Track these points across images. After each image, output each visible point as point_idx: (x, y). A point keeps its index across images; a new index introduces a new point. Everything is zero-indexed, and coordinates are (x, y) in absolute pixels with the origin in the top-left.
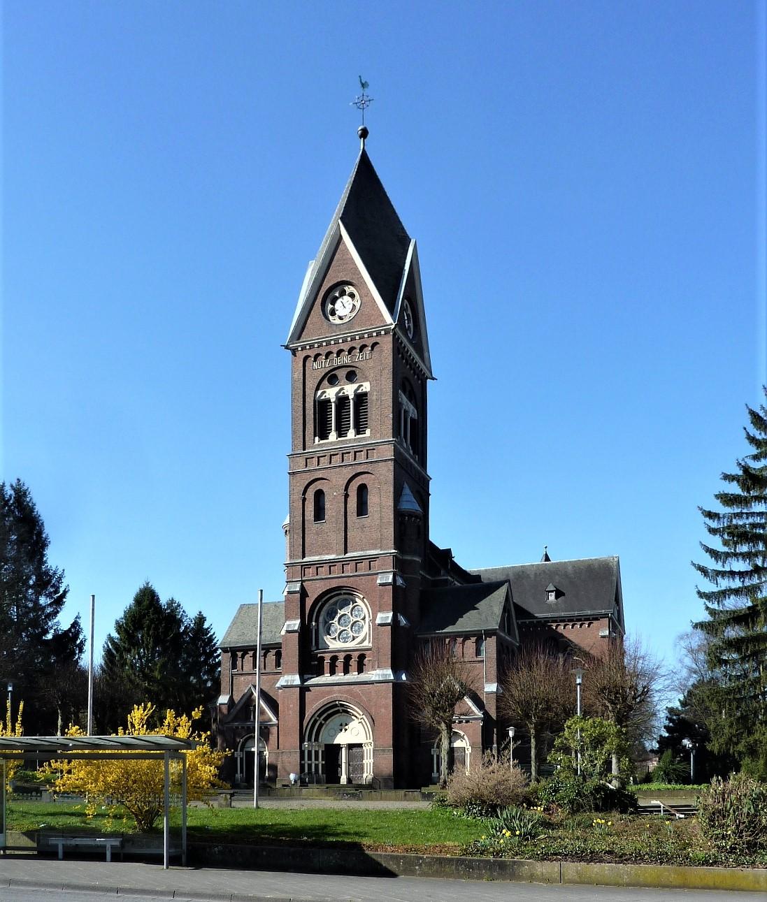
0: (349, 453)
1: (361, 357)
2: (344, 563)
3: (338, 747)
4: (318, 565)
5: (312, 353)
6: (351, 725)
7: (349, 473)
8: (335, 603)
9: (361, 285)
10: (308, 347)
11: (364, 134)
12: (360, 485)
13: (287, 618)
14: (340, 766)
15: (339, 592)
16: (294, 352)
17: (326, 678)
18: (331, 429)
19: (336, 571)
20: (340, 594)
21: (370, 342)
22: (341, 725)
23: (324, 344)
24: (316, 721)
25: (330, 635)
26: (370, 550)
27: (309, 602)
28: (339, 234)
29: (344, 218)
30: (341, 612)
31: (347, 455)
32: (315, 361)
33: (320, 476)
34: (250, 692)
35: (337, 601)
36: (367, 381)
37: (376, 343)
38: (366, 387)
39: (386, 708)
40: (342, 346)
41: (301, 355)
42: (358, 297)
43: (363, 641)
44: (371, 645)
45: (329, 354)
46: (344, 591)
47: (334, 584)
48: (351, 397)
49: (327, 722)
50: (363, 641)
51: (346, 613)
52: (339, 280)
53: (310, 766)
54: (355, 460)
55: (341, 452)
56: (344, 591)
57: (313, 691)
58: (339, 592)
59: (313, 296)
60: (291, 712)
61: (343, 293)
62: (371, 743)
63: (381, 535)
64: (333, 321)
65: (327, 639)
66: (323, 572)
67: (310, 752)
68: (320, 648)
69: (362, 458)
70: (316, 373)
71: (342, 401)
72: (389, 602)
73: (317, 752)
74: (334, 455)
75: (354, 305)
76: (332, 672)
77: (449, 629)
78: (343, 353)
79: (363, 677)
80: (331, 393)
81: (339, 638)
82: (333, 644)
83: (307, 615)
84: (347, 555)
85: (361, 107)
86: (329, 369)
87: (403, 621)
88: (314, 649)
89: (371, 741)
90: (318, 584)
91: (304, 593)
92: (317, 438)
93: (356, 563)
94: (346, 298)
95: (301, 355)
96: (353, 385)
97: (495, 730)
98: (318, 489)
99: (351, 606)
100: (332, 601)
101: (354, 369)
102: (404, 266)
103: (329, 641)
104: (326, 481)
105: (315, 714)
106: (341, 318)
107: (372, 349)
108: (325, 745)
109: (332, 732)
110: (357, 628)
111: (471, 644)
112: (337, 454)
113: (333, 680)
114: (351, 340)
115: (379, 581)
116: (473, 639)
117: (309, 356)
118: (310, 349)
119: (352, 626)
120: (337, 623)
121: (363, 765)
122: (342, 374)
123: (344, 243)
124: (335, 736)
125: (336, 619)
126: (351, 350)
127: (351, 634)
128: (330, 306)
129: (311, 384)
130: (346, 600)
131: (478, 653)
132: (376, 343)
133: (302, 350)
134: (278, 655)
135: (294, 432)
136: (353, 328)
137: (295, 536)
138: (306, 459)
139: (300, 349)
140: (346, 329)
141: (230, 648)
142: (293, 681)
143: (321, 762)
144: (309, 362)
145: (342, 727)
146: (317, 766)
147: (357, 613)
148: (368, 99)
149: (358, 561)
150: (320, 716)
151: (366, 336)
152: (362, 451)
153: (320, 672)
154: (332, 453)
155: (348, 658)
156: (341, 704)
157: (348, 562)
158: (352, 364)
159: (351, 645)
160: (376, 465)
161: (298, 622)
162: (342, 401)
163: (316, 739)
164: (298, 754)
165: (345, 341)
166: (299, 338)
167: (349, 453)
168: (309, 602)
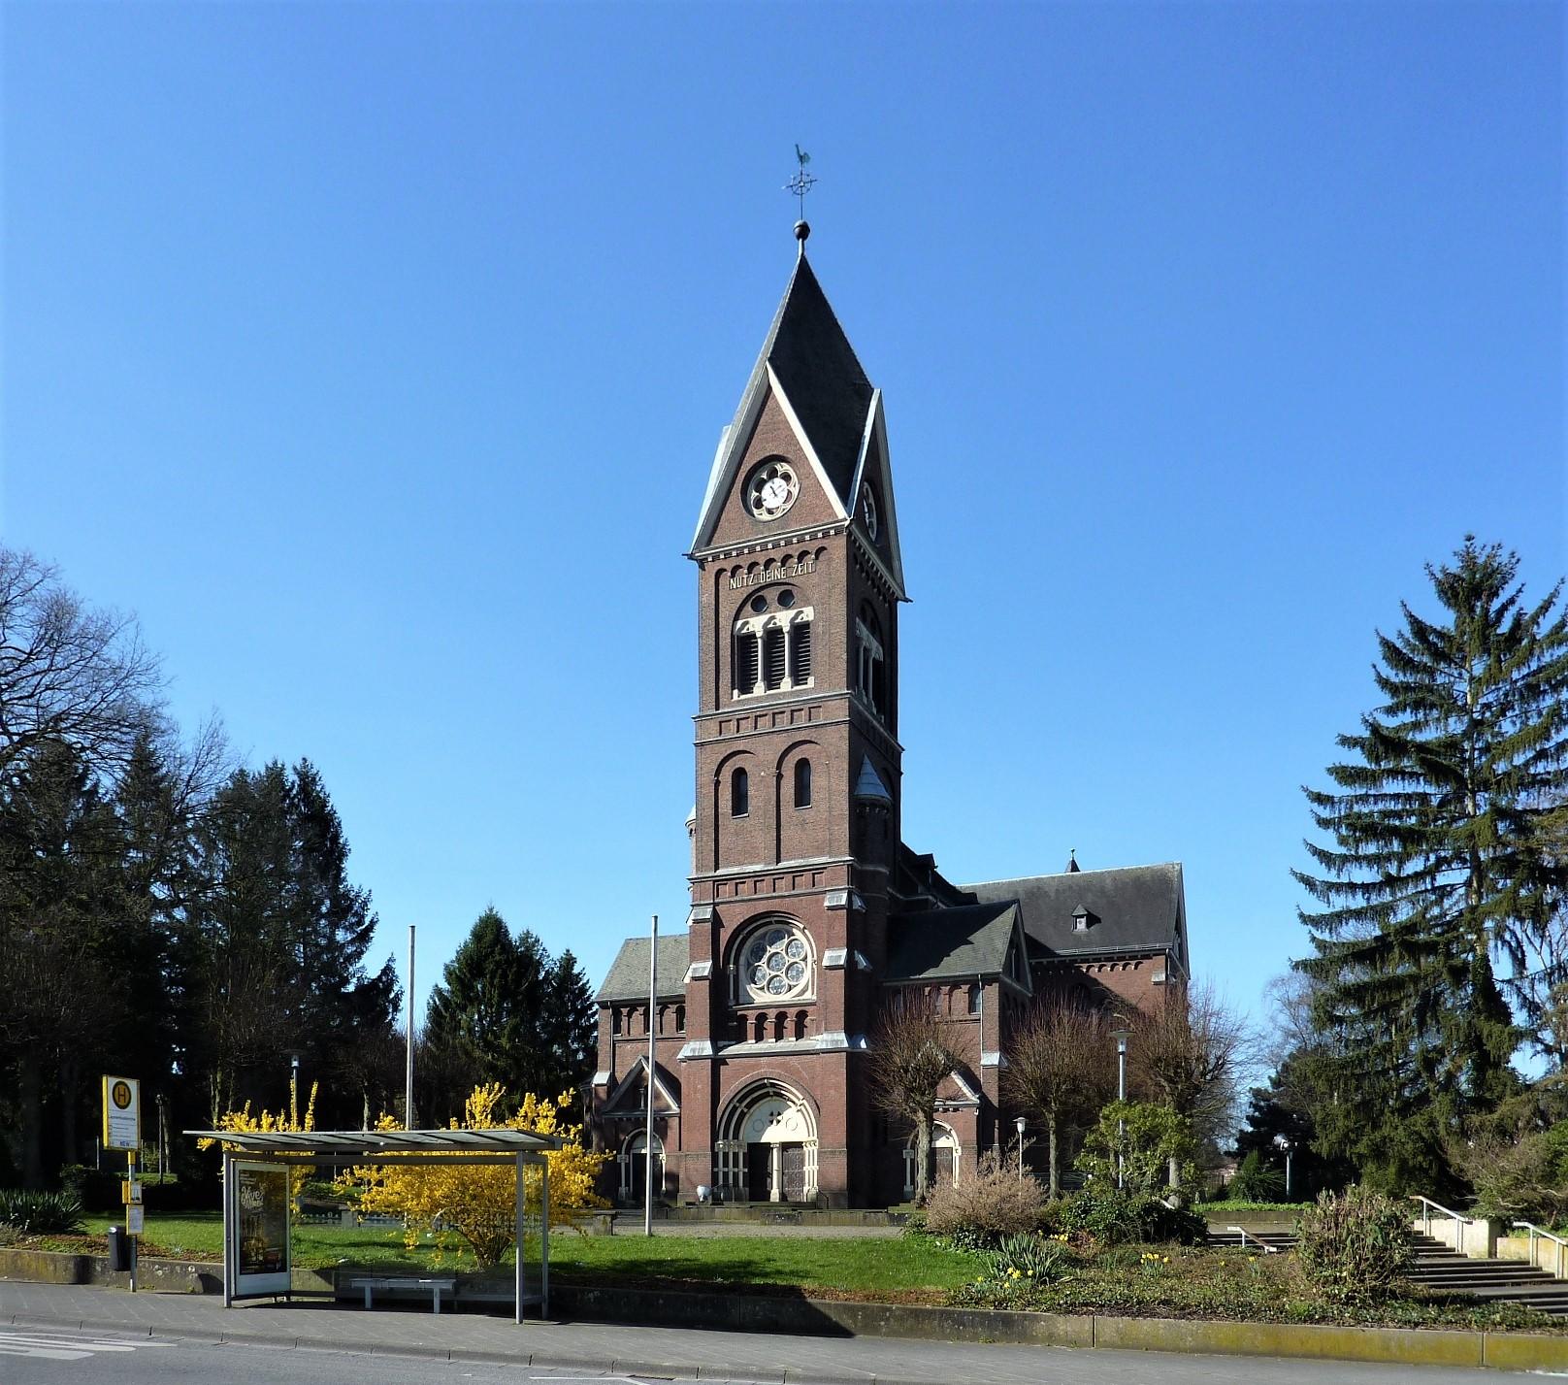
0: (783, 712)
2: (778, 876)
3: (768, 1147)
4: (738, 880)
5: (728, 565)
6: (786, 1115)
7: (783, 742)
10: (722, 557)
11: (804, 232)
13: (693, 959)
14: (770, 1175)
15: (768, 920)
17: (749, 1046)
19: (765, 887)
20: (770, 923)
21: (813, 547)
22: (772, 1114)
23: (746, 551)
24: (735, 1108)
27: (725, 936)
30: (771, 950)
31: (780, 716)
35: (766, 933)
38: (808, 614)
40: (772, 554)
41: (712, 568)
43: (804, 991)
44: (815, 998)
45: (752, 566)
46: (776, 919)
49: (752, 1111)
50: (804, 991)
51: (778, 951)
53: (726, 1175)
55: (754, 714)
56: (776, 919)
58: (768, 920)
59: (729, 480)
60: (699, 1096)
61: (773, 474)
66: (746, 889)
67: (726, 1155)
68: (741, 1002)
69: (801, 720)
71: (773, 635)
73: (736, 1155)
74: (760, 716)
75: (789, 492)
76: (759, 1038)
77: (930, 973)
78: (774, 563)
79: (804, 1044)
80: (756, 624)
82: (760, 997)
84: (780, 865)
85: (799, 192)
87: (862, 962)
89: (815, 1138)
90: (738, 908)
91: (717, 922)
92: (736, 692)
93: (737, 884)
94: (778, 482)
95: (712, 568)
96: (790, 611)
97: (997, 1121)
99: (786, 941)
100: (757, 934)
101: (789, 587)
102: (864, 430)
103: (755, 993)
105: (734, 1098)
106: (770, 511)
107: (817, 558)
109: (758, 1125)
111: (961, 995)
112: (766, 715)
113: (761, 1049)
115: (826, 904)
116: (965, 988)
119: (788, 969)
120: (765, 966)
121: (803, 1173)
122: (771, 595)
124: (762, 1131)
125: (765, 959)
126: (787, 558)
127: (786, 981)
128: (755, 494)
130: (778, 931)
131: (972, 1007)
132: (823, 549)
135: (702, 683)
136: (788, 525)
138: (721, 722)
139: (710, 559)
140: (778, 528)
141: (611, 1002)
142: (703, 1049)
143: (742, 1170)
145: (773, 1117)
146: (736, 1176)
147: (794, 950)
149: (796, 873)
150: (740, 1101)
152: (802, 710)
153: (741, 1038)
154: (758, 713)
155: (781, 1017)
157: (781, 876)
158: (787, 581)
159: (785, 998)
160: (822, 730)
162: (773, 635)
163: (736, 1136)
166: (709, 543)
167: (783, 712)
168: (725, 936)
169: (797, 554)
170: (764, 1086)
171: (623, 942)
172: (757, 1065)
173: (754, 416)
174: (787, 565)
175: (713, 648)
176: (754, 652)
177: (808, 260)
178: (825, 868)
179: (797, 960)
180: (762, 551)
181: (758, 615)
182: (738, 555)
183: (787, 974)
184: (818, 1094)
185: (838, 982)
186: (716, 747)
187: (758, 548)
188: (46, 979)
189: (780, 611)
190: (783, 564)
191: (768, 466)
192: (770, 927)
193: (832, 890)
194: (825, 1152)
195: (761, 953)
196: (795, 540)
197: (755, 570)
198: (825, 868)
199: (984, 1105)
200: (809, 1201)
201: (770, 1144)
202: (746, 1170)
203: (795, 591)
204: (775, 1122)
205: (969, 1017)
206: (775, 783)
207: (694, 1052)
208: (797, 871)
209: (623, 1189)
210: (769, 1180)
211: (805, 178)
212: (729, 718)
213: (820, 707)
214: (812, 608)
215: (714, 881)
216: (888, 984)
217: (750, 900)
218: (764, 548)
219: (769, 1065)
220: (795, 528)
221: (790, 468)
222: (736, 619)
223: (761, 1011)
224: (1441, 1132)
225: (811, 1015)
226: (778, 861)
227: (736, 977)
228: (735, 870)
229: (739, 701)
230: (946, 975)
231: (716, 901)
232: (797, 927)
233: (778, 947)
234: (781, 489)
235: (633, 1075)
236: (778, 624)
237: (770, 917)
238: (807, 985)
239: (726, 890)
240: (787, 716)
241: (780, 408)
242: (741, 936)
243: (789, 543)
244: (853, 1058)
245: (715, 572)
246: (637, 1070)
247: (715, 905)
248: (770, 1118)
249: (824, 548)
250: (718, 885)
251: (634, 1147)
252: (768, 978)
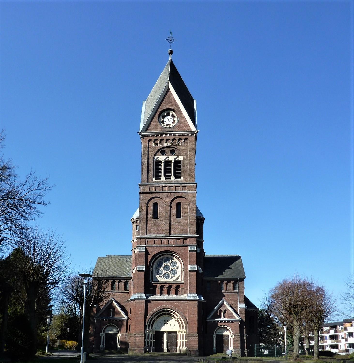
0: (173, 187)
2: (170, 239)
3: (163, 332)
4: (156, 239)
5: (153, 139)
6: (170, 322)
7: (173, 196)
8: (162, 259)
10: (151, 136)
12: (180, 202)
14: (163, 343)
15: (165, 253)
16: (143, 137)
17: (158, 296)
18: (171, 175)
19: (165, 243)
20: (166, 255)
22: (165, 321)
24: (153, 318)
25: (159, 275)
26: (183, 234)
27: (150, 257)
30: (165, 264)
31: (171, 188)
32: (154, 142)
33: (157, 196)
34: (111, 301)
35: (163, 258)
38: (181, 158)
40: (169, 138)
41: (147, 139)
44: (183, 281)
45: (161, 140)
46: (168, 253)
47: (164, 249)
48: (173, 161)
49: (158, 319)
51: (168, 264)
52: (167, 108)
53: (148, 342)
54: (176, 190)
55: (162, 186)
56: (168, 253)
57: (152, 302)
58: (165, 253)
59: (154, 113)
61: (168, 114)
62: (185, 331)
63: (189, 227)
65: (158, 277)
66: (158, 242)
67: (148, 334)
69: (179, 189)
70: (154, 148)
71: (167, 163)
73: (151, 335)
74: (164, 187)
75: (174, 121)
76: (161, 294)
77: (220, 277)
78: (169, 141)
80: (162, 158)
81: (164, 277)
82: (161, 280)
83: (148, 264)
84: (171, 236)
85: (170, 41)
86: (162, 147)
87: (201, 271)
88: (151, 281)
89: (185, 330)
90: (155, 248)
91: (147, 253)
92: (154, 178)
93: (154, 240)
94: (170, 117)
95: (147, 139)
97: (245, 327)
98: (155, 202)
99: (171, 261)
101: (174, 149)
103: (159, 278)
105: (152, 315)
106: (167, 125)
107: (184, 141)
111: (231, 285)
112: (166, 187)
114: (174, 136)
115: (189, 250)
116: (233, 282)
118: (152, 136)
119: (171, 271)
121: (177, 343)
122: (168, 150)
123: (170, 92)
124: (162, 327)
125: (163, 267)
126: (174, 140)
127: (171, 275)
128: (162, 119)
129: (152, 153)
130: (167, 258)
131: (235, 289)
133: (147, 136)
134: (126, 283)
135: (142, 174)
137: (142, 224)
139: (146, 136)
140: (171, 130)
142: (142, 297)
143: (153, 340)
145: (166, 322)
146: (151, 342)
147: (173, 265)
149: (177, 239)
150: (155, 316)
152: (179, 187)
153: (154, 293)
155: (170, 287)
156: (167, 310)
157: (172, 239)
158: (174, 146)
159: (170, 280)
161: (144, 266)
162: (167, 163)
163: (152, 328)
164: (144, 335)
165: (170, 135)
166: (146, 130)
167: (173, 187)
168: (150, 257)
169: (178, 139)
170: (165, 311)
173: (163, 96)
174: (174, 142)
175: (147, 163)
177: (173, 61)
179: (175, 268)
180: (165, 136)
182: (156, 136)
183: (171, 272)
185: (194, 278)
186: (148, 195)
187: (164, 135)
188: (24, 231)
193: (190, 245)
194: (190, 335)
195: (161, 265)
197: (174, 141)
198: (188, 238)
199: (241, 321)
201: (164, 331)
202: (154, 340)
204: (166, 324)
207: (139, 297)
209: (102, 346)
210: (163, 344)
212: (153, 186)
213: (186, 187)
215: (146, 239)
216: (205, 279)
218: (166, 135)
219: (167, 304)
220: (177, 131)
221: (175, 113)
222: (155, 155)
223: (162, 284)
224: (103, 303)
225: (182, 287)
226: (170, 234)
227: (152, 272)
228: (154, 236)
231: (147, 245)
232: (176, 257)
233: (168, 263)
234: (171, 119)
235: (108, 304)
236: (170, 159)
237: (166, 252)
239: (151, 242)
240: (174, 188)
241: (172, 95)
242: (155, 258)
243: (170, 135)
244: (199, 302)
245: (148, 140)
247: (146, 246)
248: (164, 322)
249: (187, 139)
250: (147, 240)
251: (105, 330)
252: (164, 273)
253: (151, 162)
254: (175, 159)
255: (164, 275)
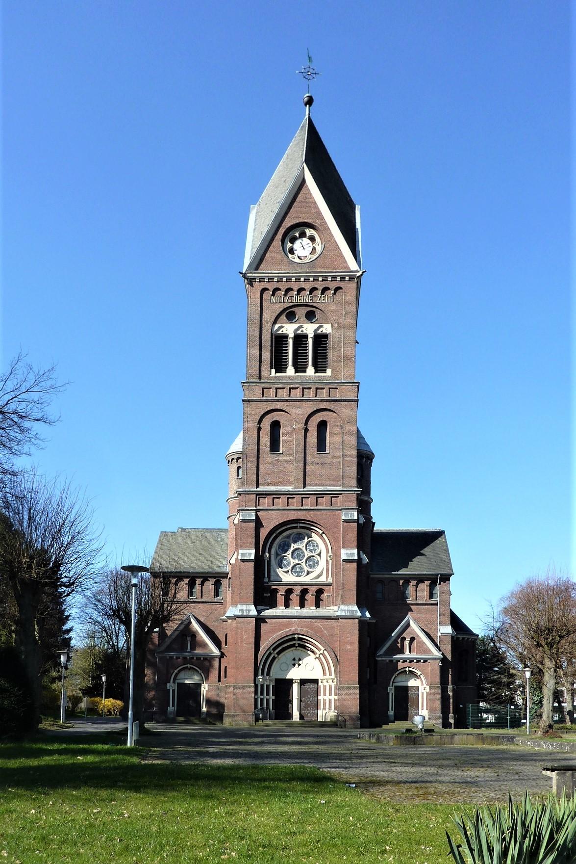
0: (310, 388)
1: (322, 299)
2: (305, 496)
3: (291, 681)
4: (276, 495)
5: (271, 286)
7: (310, 408)
8: (288, 537)
9: (322, 228)
10: (267, 280)
11: (310, 102)
13: (238, 547)
14: (291, 702)
16: (251, 282)
17: (280, 610)
19: (295, 503)
20: (296, 527)
21: (333, 285)
23: (285, 279)
24: (270, 654)
25: (282, 568)
27: (264, 533)
28: (302, 176)
29: (306, 161)
30: (294, 546)
31: (307, 390)
32: (273, 294)
33: (278, 407)
35: (290, 535)
36: (328, 323)
37: (340, 288)
38: (327, 328)
39: (351, 644)
40: (303, 285)
41: (258, 286)
42: (319, 240)
43: (319, 576)
44: (330, 580)
45: (289, 290)
46: (301, 525)
47: (293, 516)
49: (280, 656)
50: (319, 576)
51: (300, 547)
52: (301, 221)
53: (262, 700)
54: (316, 396)
55: (289, 386)
56: (301, 525)
61: (303, 235)
64: (293, 260)
65: (280, 571)
66: (281, 503)
67: (262, 686)
68: (272, 580)
70: (273, 307)
71: (300, 339)
72: (353, 539)
73: (268, 686)
74: (293, 388)
75: (314, 249)
77: (403, 571)
78: (304, 292)
79: (322, 611)
80: (289, 329)
81: (292, 572)
82: (287, 577)
84: (306, 489)
86: (288, 305)
87: (366, 560)
88: (266, 580)
89: (333, 676)
90: (275, 515)
91: (258, 523)
92: (273, 371)
93: (274, 498)
94: (305, 241)
95: (258, 286)
96: (313, 324)
97: (450, 670)
98: (274, 419)
99: (306, 541)
100: (285, 534)
101: (314, 309)
102: (355, 226)
104: (284, 413)
106: (299, 258)
107: (335, 293)
108: (276, 679)
109: (284, 667)
110: (311, 563)
111: (424, 587)
112: (297, 388)
113: (291, 613)
115: (343, 517)
116: (427, 583)
117: (267, 289)
118: (269, 282)
119: (307, 560)
120: (290, 556)
122: (301, 312)
124: (288, 670)
125: (290, 552)
127: (306, 568)
128: (289, 245)
129: (268, 317)
130: (300, 534)
131: (431, 596)
132: (340, 288)
133: (260, 282)
135: (249, 361)
136: (314, 268)
137: (249, 465)
138: (263, 388)
139: (257, 280)
141: (163, 573)
142: (249, 611)
143: (272, 697)
144: (267, 295)
145: (296, 661)
146: (268, 700)
147: (311, 548)
148: (314, 72)
149: (319, 495)
150: (274, 649)
151: (329, 279)
152: (323, 388)
153: (273, 605)
154: (292, 386)
155: (304, 592)
156: (298, 638)
157: (308, 496)
158: (313, 304)
161: (253, 551)
162: (300, 339)
163: (268, 674)
165: (307, 280)
166: (257, 268)
167: (310, 388)
168: (264, 533)
170: (294, 639)
171: (160, 533)
172: (290, 624)
174: (313, 294)
175: (258, 339)
176: (305, 341)
178: (341, 494)
181: (290, 323)
183: (306, 563)
184: (337, 647)
186: (260, 404)
187: (293, 280)
189: (307, 323)
190: (311, 293)
191: (301, 229)
192: (295, 530)
194: (343, 687)
196: (320, 279)
197: (290, 293)
198: (341, 494)
200: (329, 720)
201: (292, 680)
203: (317, 312)
204: (297, 665)
205: (429, 602)
206: (303, 434)
207: (243, 612)
208: (335, 494)
211: (311, 71)
212: (270, 386)
213: (337, 388)
214: (330, 325)
215: (257, 495)
217: (284, 510)
219: (299, 625)
222: (275, 323)
229: (276, 377)
230: (416, 573)
231: (258, 508)
233: (301, 545)
234: (309, 245)
236: (305, 332)
237: (297, 523)
238: (322, 572)
239: (266, 502)
240: (313, 391)
241: (311, 194)
246: (186, 623)
247: (257, 511)
248: (293, 662)
250: (259, 498)
251: (177, 678)
253: (267, 337)
254: (316, 330)
255: (292, 569)
